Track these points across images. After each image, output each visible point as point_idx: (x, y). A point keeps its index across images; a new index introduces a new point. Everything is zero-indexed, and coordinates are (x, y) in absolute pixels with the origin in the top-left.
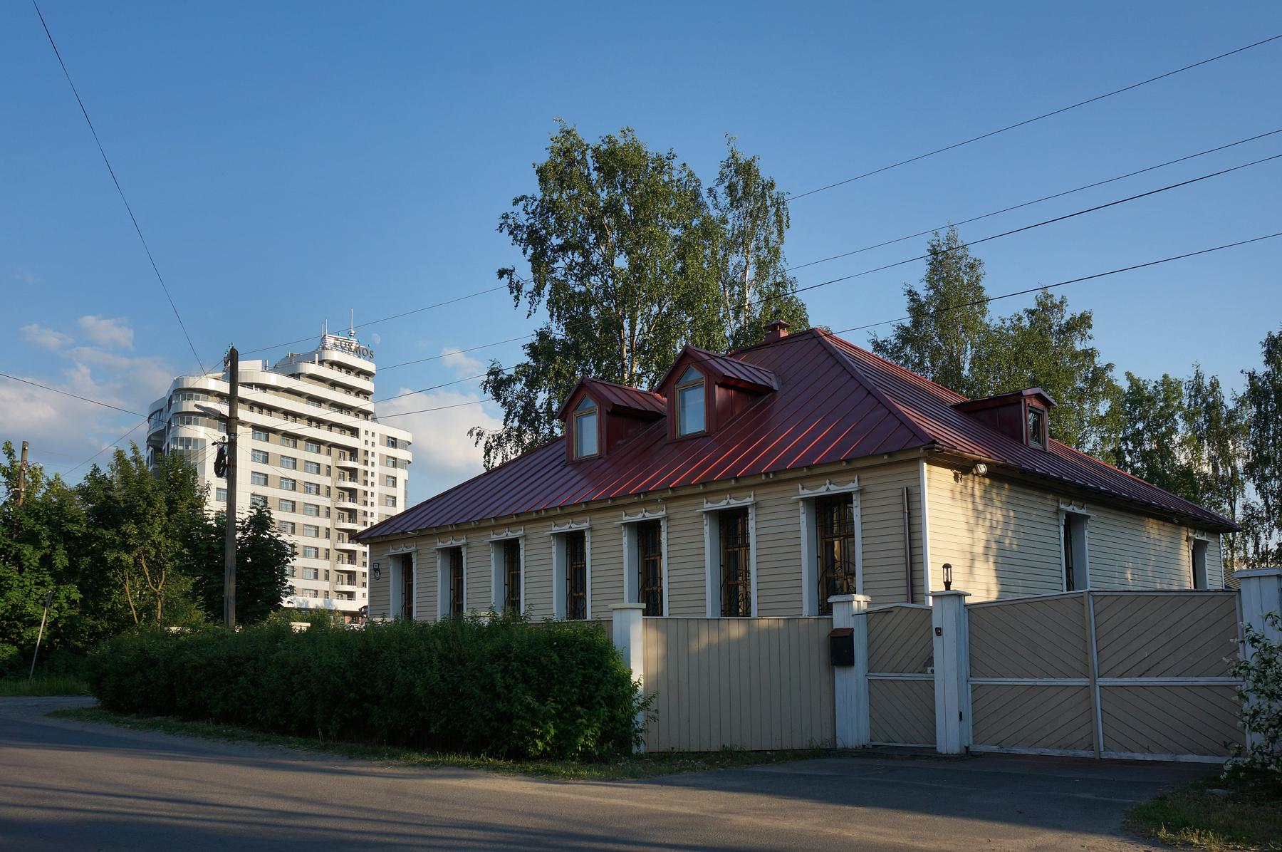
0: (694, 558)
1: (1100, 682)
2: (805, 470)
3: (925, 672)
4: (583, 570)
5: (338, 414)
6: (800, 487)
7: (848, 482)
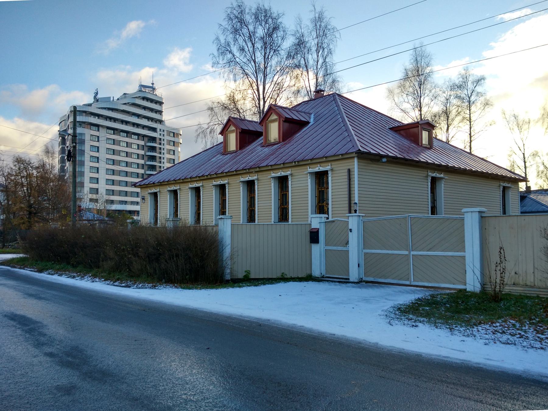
0: (237, 199)
1: (412, 253)
2: (340, 156)
3: (347, 247)
4: (254, 198)
5: (132, 128)
6: (308, 167)
7: (327, 166)
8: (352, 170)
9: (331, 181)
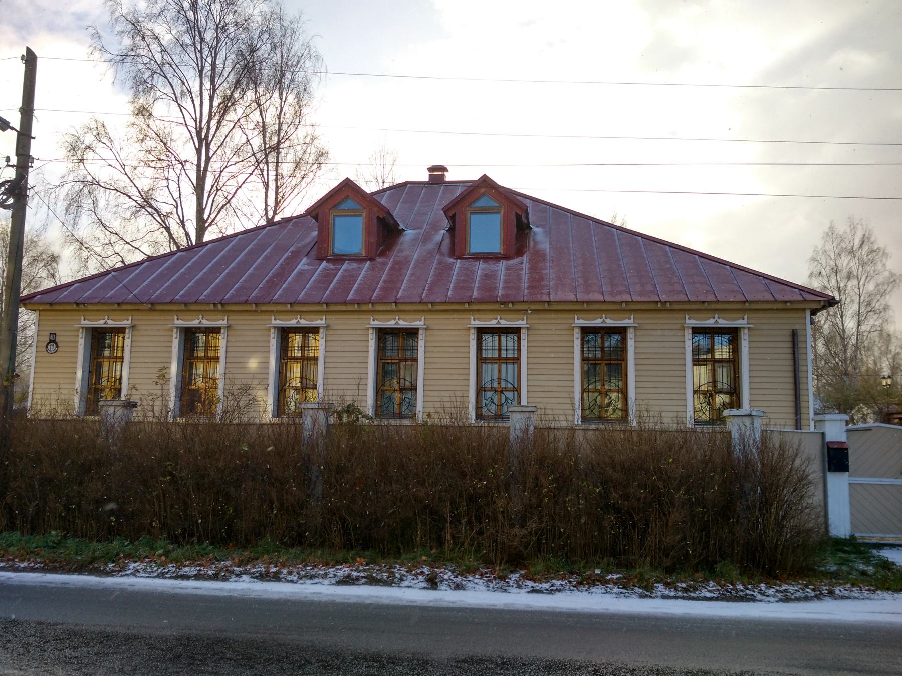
7: (416, 320)
8: (800, 333)
9: (129, 347)
